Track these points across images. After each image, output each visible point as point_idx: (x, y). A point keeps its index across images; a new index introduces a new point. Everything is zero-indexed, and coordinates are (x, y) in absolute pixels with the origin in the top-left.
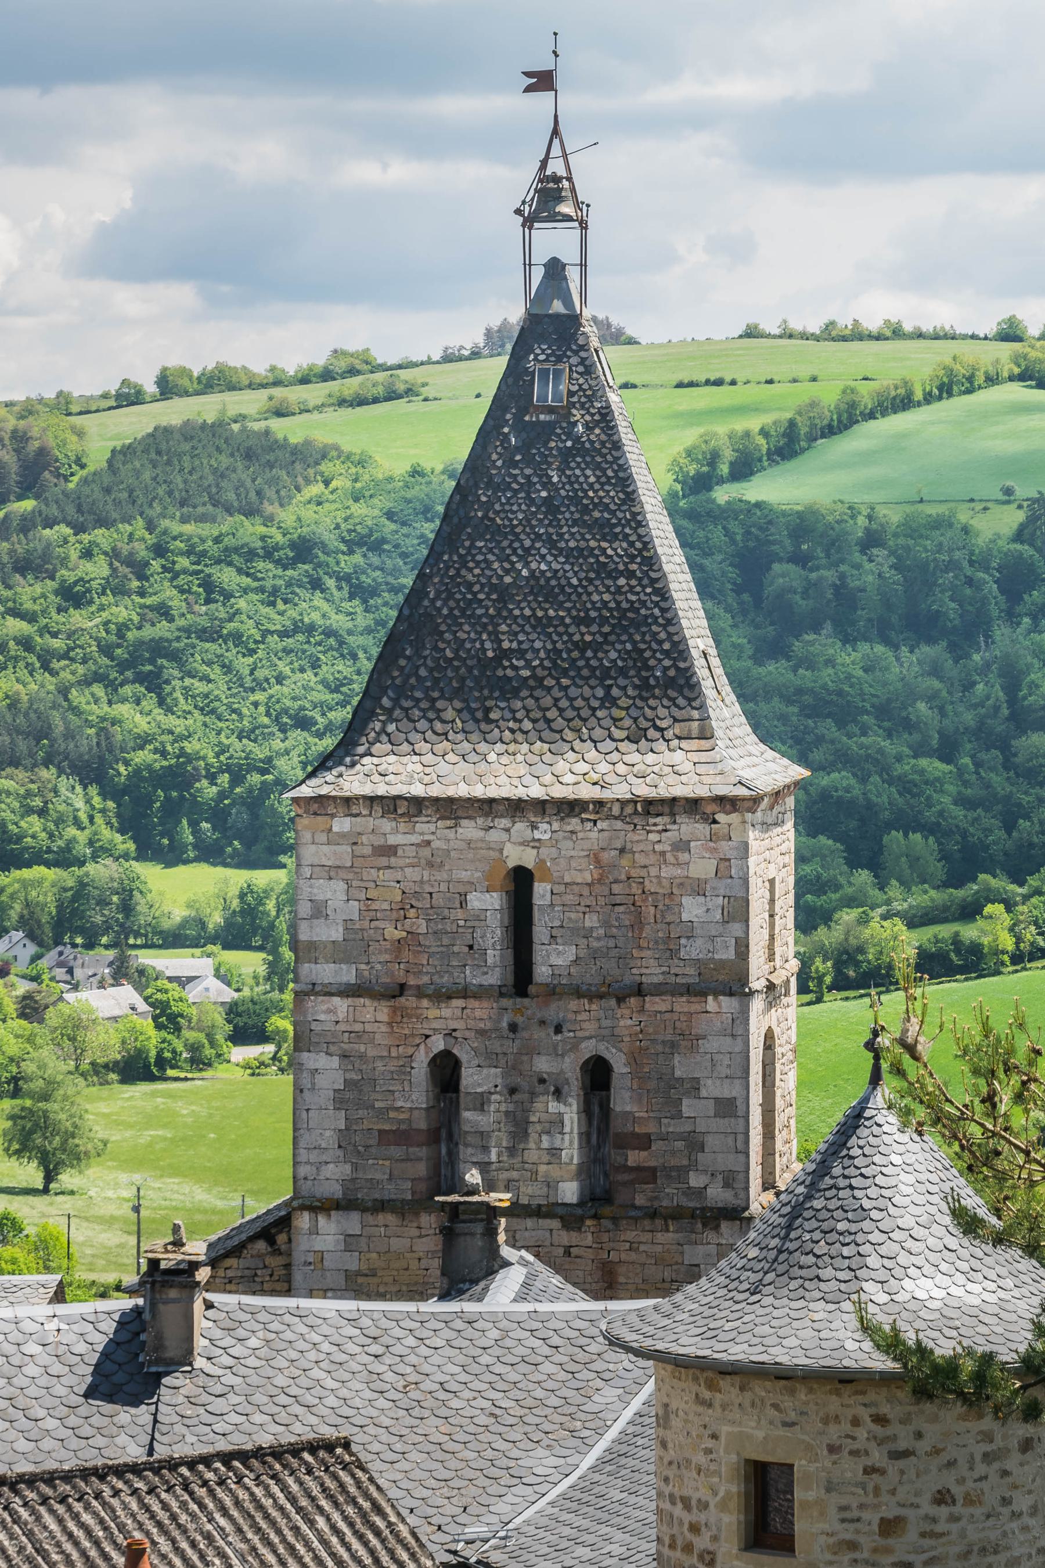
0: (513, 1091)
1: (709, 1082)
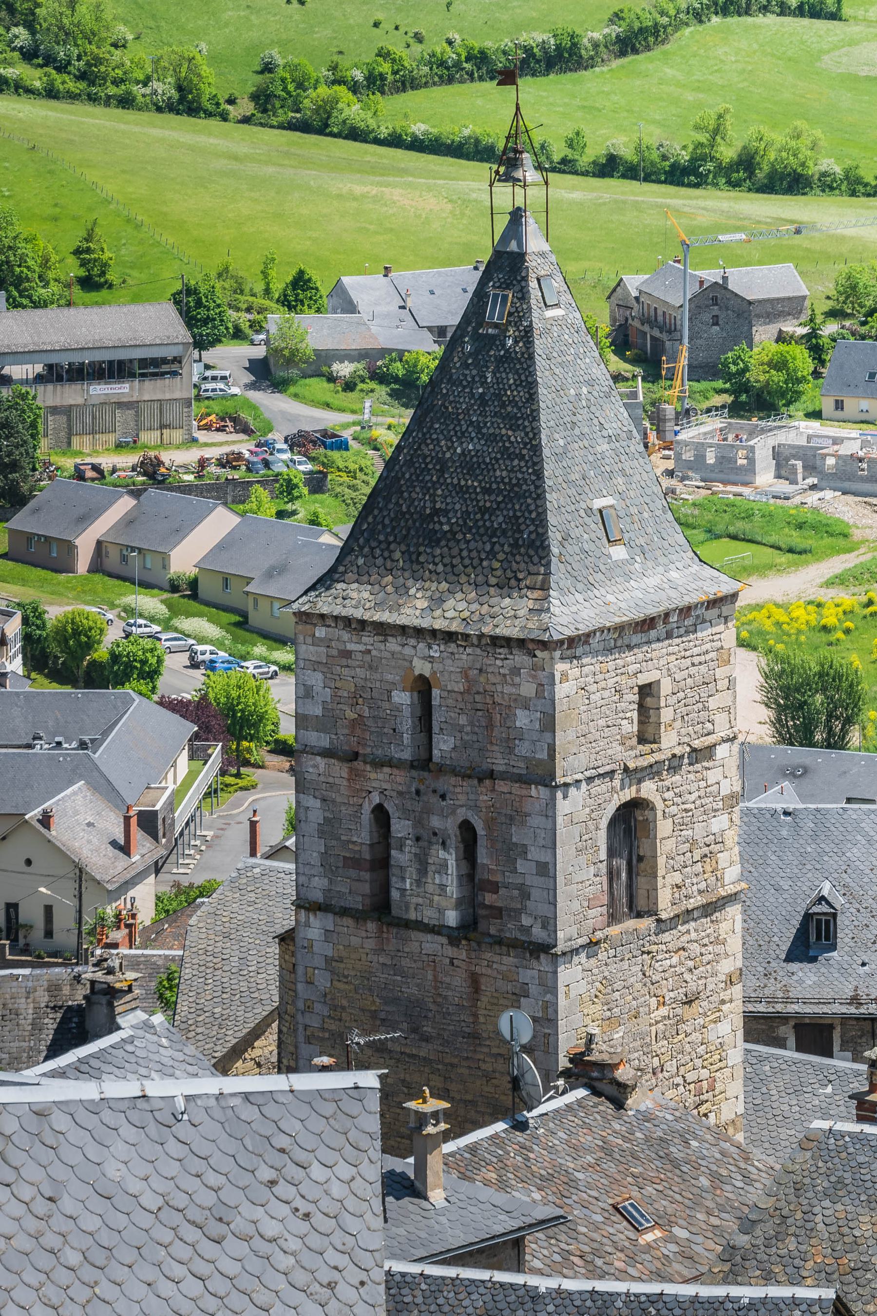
0: (418, 839)
1: (533, 848)
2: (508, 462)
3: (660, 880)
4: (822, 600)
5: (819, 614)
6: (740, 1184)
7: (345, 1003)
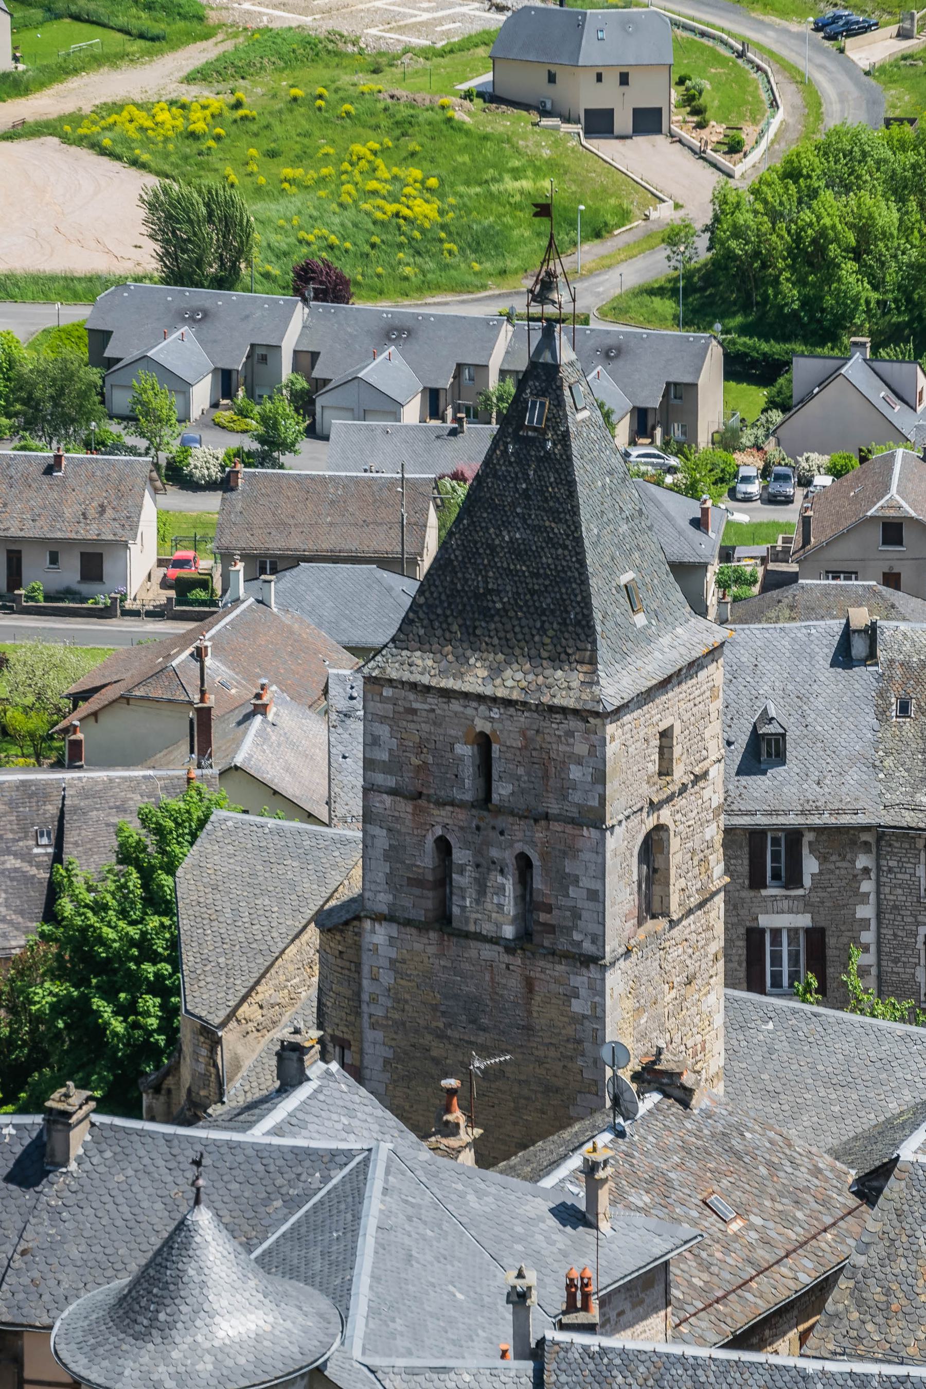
0: (478, 866)
2: (553, 551)
3: (671, 887)
4: (185, 99)
5: (187, 118)
6: (790, 1170)
7: (407, 997)
